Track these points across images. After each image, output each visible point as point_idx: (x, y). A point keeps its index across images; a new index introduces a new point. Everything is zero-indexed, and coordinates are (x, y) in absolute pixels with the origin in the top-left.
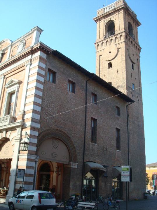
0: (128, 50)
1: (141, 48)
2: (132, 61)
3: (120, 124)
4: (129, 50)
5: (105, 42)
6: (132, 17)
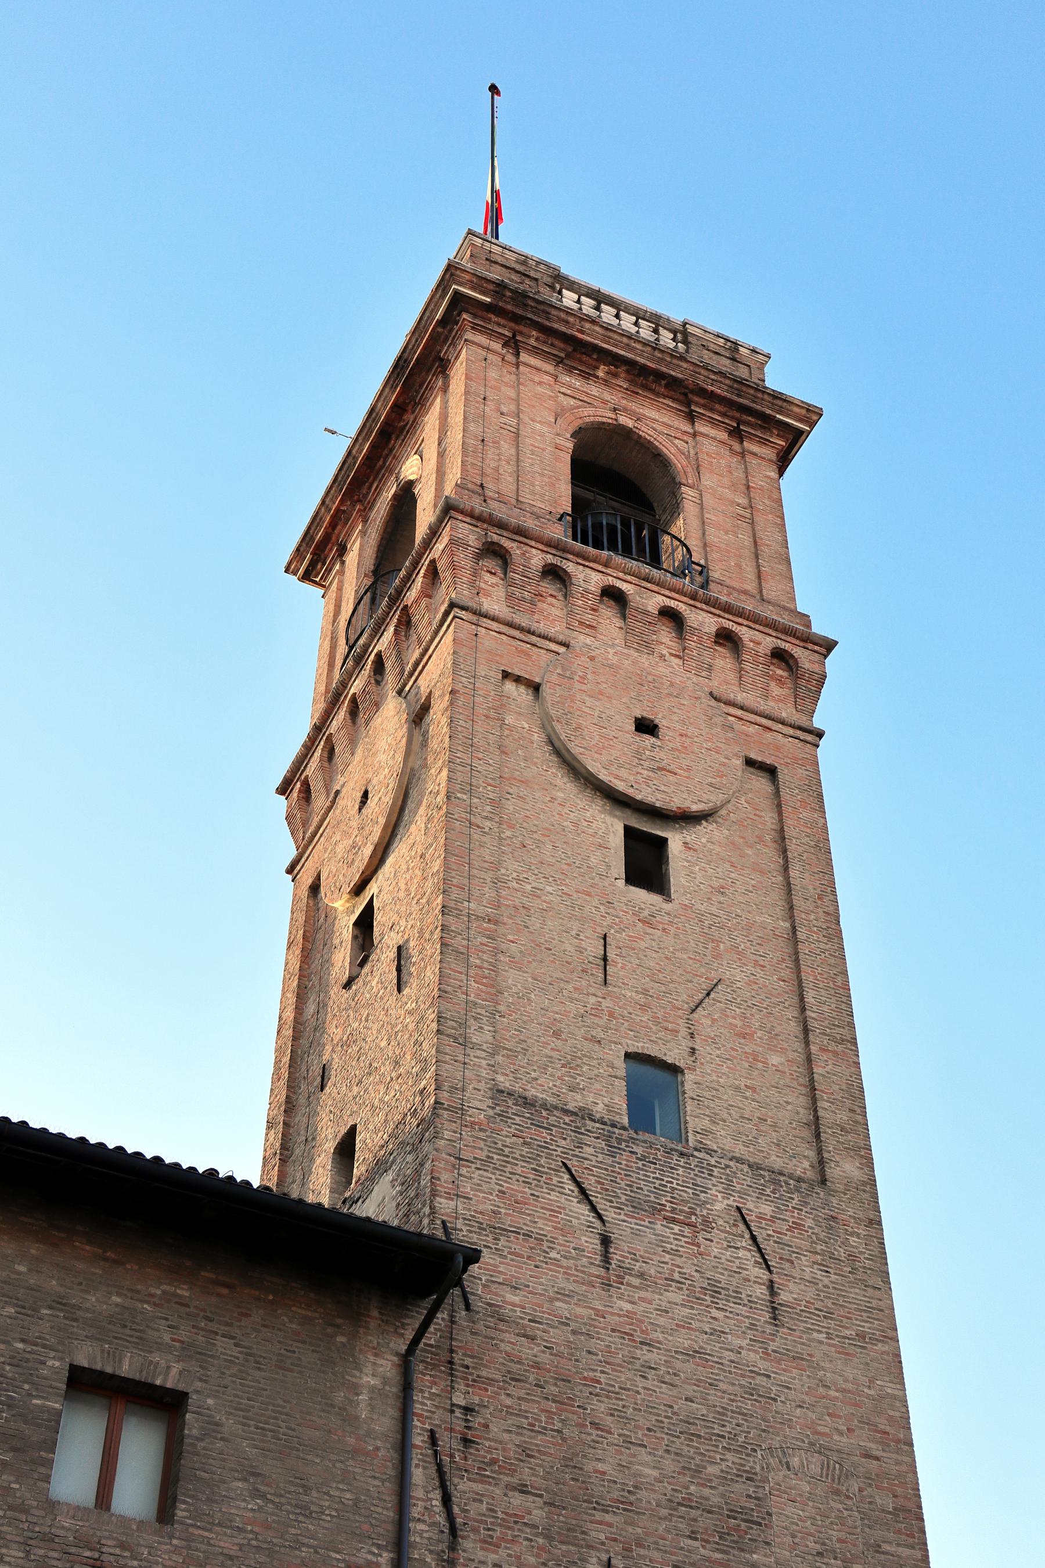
6: (630, 364)
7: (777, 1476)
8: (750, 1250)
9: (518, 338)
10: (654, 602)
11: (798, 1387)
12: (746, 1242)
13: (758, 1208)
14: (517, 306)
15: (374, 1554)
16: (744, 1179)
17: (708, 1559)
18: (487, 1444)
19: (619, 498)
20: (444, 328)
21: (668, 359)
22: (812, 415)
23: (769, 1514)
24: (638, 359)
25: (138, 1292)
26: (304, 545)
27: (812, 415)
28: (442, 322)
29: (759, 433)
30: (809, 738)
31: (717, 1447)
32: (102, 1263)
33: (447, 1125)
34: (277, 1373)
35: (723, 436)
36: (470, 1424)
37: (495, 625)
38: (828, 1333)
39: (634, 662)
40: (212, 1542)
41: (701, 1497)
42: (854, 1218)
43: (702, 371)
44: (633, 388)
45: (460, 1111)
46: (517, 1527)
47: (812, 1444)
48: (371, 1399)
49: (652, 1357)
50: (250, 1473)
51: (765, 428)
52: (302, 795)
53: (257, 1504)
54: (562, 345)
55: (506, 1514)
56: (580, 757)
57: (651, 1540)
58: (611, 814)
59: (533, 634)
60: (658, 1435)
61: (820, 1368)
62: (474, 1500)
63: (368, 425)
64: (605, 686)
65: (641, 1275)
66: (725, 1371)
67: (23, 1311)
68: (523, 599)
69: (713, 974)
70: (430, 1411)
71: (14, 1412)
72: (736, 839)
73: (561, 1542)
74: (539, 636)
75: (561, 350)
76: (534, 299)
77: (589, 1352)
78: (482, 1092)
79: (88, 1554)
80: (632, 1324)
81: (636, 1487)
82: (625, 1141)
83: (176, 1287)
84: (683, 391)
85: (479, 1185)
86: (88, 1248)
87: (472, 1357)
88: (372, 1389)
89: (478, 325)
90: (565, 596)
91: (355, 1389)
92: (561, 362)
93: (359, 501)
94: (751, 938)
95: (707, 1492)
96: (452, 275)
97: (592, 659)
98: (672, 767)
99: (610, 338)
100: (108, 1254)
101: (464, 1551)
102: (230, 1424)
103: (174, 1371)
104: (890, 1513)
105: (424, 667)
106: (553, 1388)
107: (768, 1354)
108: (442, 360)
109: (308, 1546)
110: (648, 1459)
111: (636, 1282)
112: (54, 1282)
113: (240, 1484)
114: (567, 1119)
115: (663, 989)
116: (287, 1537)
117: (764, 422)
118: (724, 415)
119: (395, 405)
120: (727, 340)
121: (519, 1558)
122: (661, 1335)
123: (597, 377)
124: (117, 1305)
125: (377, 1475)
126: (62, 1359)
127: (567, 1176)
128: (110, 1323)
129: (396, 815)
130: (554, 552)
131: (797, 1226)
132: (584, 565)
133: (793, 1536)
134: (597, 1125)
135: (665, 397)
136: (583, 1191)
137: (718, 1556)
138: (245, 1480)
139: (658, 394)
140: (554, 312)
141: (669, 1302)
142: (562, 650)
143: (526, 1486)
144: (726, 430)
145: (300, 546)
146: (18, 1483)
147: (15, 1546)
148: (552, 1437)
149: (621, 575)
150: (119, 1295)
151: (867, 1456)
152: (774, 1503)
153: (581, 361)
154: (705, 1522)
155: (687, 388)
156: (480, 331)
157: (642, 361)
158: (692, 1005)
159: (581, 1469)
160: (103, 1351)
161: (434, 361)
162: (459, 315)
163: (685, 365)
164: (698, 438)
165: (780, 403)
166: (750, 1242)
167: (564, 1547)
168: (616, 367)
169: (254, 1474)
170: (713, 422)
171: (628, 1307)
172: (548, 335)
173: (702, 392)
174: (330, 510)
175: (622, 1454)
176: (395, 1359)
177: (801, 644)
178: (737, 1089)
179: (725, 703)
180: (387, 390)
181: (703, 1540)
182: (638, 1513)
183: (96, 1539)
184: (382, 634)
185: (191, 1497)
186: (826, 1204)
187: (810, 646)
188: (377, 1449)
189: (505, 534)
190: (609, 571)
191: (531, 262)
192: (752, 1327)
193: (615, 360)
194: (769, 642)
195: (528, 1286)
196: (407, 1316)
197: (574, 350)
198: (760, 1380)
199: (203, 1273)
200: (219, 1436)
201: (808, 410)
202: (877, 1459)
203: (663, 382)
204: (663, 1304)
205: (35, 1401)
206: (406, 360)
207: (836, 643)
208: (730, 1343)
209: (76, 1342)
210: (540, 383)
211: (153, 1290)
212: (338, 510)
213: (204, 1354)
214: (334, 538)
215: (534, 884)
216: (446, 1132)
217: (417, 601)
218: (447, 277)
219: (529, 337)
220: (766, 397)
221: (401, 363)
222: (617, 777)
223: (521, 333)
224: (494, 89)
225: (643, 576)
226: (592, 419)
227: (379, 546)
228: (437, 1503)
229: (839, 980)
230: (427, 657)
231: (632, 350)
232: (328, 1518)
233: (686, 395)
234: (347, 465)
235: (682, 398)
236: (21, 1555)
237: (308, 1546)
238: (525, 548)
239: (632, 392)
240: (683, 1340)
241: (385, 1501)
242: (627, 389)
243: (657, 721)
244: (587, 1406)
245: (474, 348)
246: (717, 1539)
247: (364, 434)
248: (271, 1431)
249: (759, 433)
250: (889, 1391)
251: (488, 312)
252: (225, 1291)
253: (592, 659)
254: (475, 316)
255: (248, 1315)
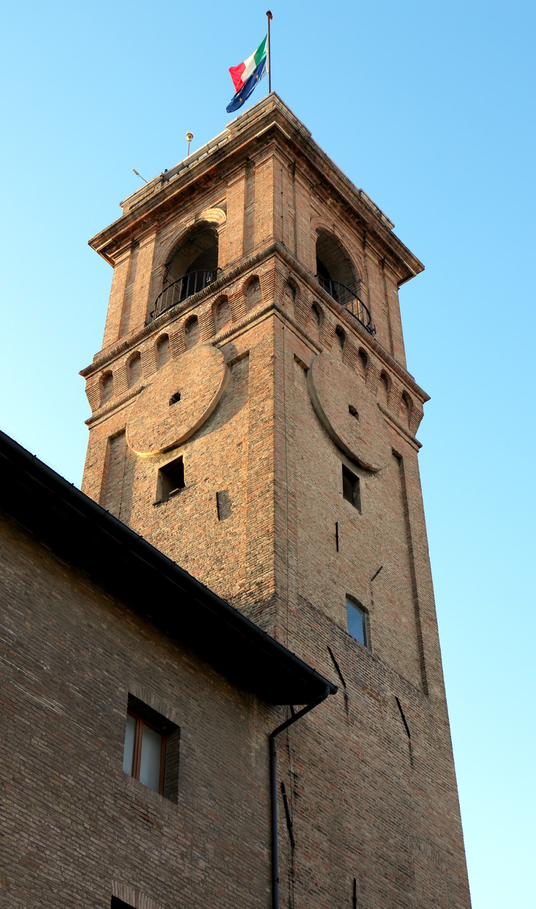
0: (306, 370)
1: (426, 398)
2: (341, 448)
3: (174, 872)
4: (315, 373)
5: (146, 347)
6: (345, 203)
7: (416, 852)
8: (401, 723)
9: (296, 165)
10: (358, 343)
11: (422, 805)
12: (399, 718)
13: (405, 702)
14: (302, 147)
15: (261, 848)
16: (397, 683)
17: (391, 890)
18: (304, 798)
19: (333, 274)
20: (257, 143)
21: (364, 209)
22: (419, 268)
23: (414, 873)
24: (350, 202)
25: (156, 659)
26: (109, 233)
27: (419, 268)
28: (258, 139)
29: (392, 267)
30: (415, 446)
31: (393, 828)
32: (139, 636)
33: (280, 608)
34: (217, 728)
35: (377, 262)
36: (297, 785)
37: (291, 326)
38: (432, 779)
39: (348, 374)
40: (195, 820)
41: (388, 855)
42: (440, 719)
43: (377, 222)
44: (341, 217)
45: (286, 601)
46: (317, 850)
47: (428, 839)
48: (256, 756)
49: (366, 770)
50: (209, 785)
51: (395, 265)
52: (101, 380)
53: (212, 803)
54: (316, 178)
55: (313, 841)
56: (328, 417)
57: (370, 873)
58: (337, 455)
59: (307, 338)
60: (371, 815)
61: (430, 798)
62: (300, 829)
63: (182, 179)
64: (336, 381)
65: (361, 722)
66: (394, 787)
67: (106, 653)
68: (302, 317)
69: (379, 562)
70: (280, 772)
71: (105, 713)
72: (386, 490)
73: (335, 864)
74: (309, 341)
75: (315, 181)
76: (311, 147)
77: (342, 759)
78: (293, 594)
79: (142, 810)
80: (358, 749)
81: (363, 842)
82: (352, 644)
83: (172, 662)
84: (364, 229)
85: (295, 647)
86: (133, 624)
87: (296, 746)
88: (256, 751)
89: (279, 149)
90: (319, 322)
91: (249, 748)
92: (312, 188)
93: (158, 220)
94: (393, 548)
95: (390, 853)
96: (276, 115)
97: (331, 364)
98: (364, 439)
99: (340, 185)
100: (142, 631)
101: (297, 857)
102: (198, 752)
103: (174, 712)
104: (457, 886)
105: (239, 335)
106: (328, 775)
107: (410, 783)
108: (248, 160)
109: (235, 835)
110: (367, 827)
111: (359, 725)
112: (119, 640)
113: (204, 789)
114: (328, 623)
115: (360, 563)
116: (225, 826)
117: (397, 262)
118: (379, 250)
119: (206, 175)
120: (378, 209)
121: (319, 868)
122: (369, 759)
123: (327, 204)
124: (147, 664)
125: (260, 802)
126: (125, 688)
127: (329, 655)
128: (145, 673)
129: (209, 415)
130: (318, 295)
131: (418, 716)
132: (329, 309)
133: (423, 888)
134: (340, 630)
135: (355, 228)
136: (337, 666)
137: (396, 890)
138: (206, 787)
139: (352, 226)
140: (318, 158)
141: (372, 741)
142: (318, 353)
143: (320, 827)
144: (378, 259)
145: (105, 232)
146: (109, 758)
147: (109, 795)
148: (329, 803)
149: (345, 321)
150: (148, 658)
151: (449, 852)
152: (416, 866)
153: (321, 191)
154: (390, 870)
155: (367, 228)
156: (279, 153)
157: (352, 205)
158: (372, 577)
159: (341, 825)
160: (142, 690)
161: (243, 159)
162: (271, 139)
163: (370, 215)
164: (367, 258)
165: (407, 255)
166: (401, 718)
167: (336, 867)
168: (337, 202)
169: (210, 785)
170: (373, 252)
171: (356, 738)
172: (311, 170)
173: (374, 234)
174: (136, 219)
175: (357, 821)
176: (265, 736)
177: (415, 393)
178: (390, 630)
179: (383, 413)
180: (204, 164)
181: (389, 880)
182: (364, 857)
183: (145, 803)
184: (198, 305)
185: (185, 790)
186: (429, 708)
187: (418, 395)
188: (260, 786)
189: (298, 275)
190: (340, 317)
191: (299, 124)
192: (403, 766)
193: (339, 198)
194: (401, 387)
195: (316, 713)
196: (268, 713)
197: (321, 184)
198: (407, 797)
199: (183, 658)
200: (194, 757)
201: (419, 264)
202: (452, 855)
203: (357, 220)
204: (370, 741)
205: (114, 710)
206: (224, 152)
207: (430, 398)
208: (395, 772)
209: (131, 680)
210: (304, 195)
211: (162, 661)
212: (141, 221)
213: (186, 707)
214: (131, 236)
215: (308, 483)
216: (280, 612)
217: (237, 295)
218: (272, 115)
219: (302, 167)
220: (402, 249)
221: (220, 152)
222: (343, 435)
223: (298, 163)
224: (269, 14)
225: (354, 326)
226: (323, 226)
227: (171, 251)
228: (285, 826)
229: (430, 584)
230: (242, 331)
231: (349, 196)
232: (241, 821)
233: (365, 231)
234: (158, 197)
235: (362, 232)
236: (113, 802)
237: (235, 835)
238: (306, 288)
239: (341, 219)
240: (377, 764)
241: (264, 818)
242: (338, 216)
243: (357, 411)
244: (342, 789)
245: (276, 161)
246: (394, 880)
247: (178, 183)
248: (216, 762)
249: (392, 267)
250: (455, 819)
251: (286, 144)
252: (193, 672)
253: (331, 364)
254: (279, 143)
255: (203, 690)
